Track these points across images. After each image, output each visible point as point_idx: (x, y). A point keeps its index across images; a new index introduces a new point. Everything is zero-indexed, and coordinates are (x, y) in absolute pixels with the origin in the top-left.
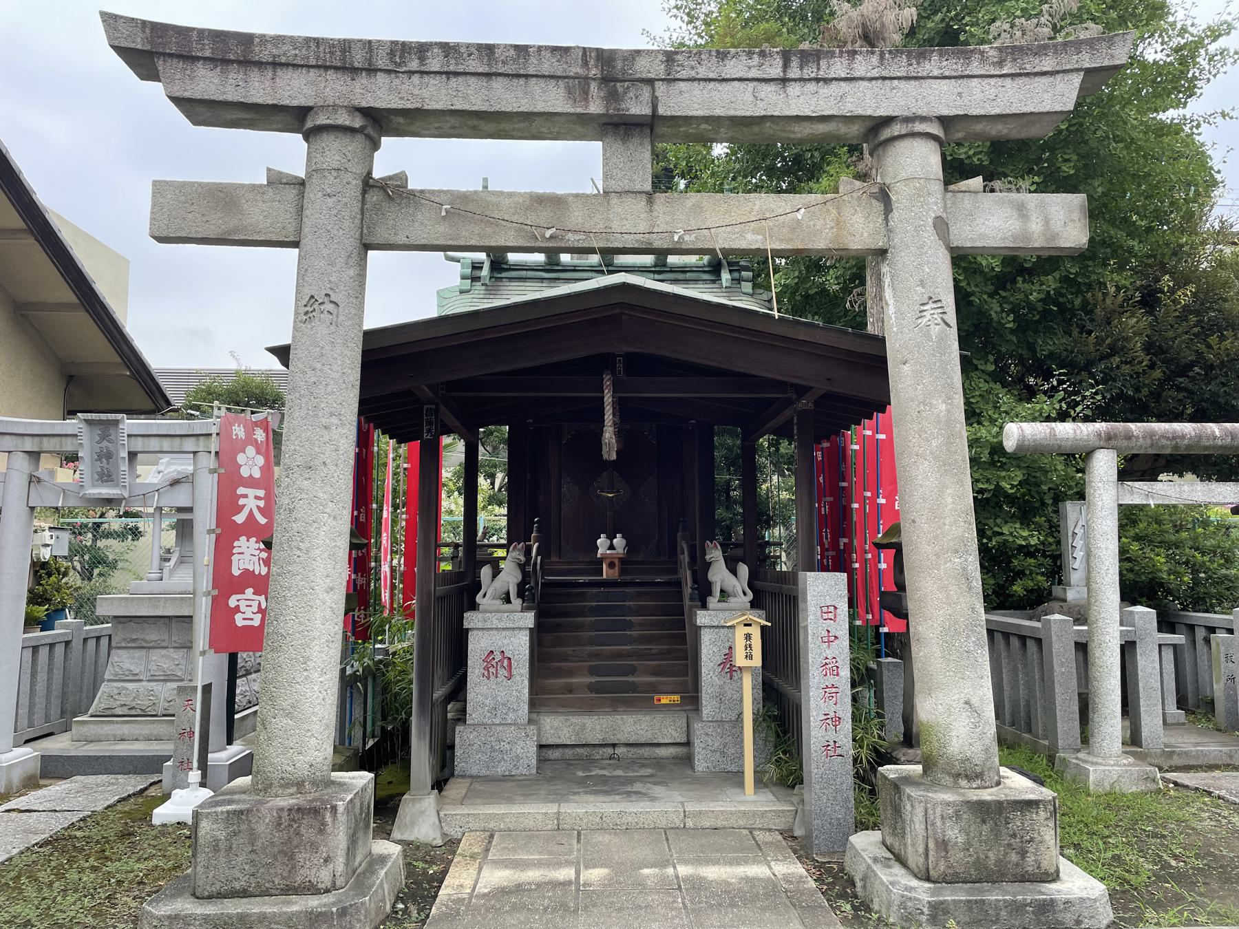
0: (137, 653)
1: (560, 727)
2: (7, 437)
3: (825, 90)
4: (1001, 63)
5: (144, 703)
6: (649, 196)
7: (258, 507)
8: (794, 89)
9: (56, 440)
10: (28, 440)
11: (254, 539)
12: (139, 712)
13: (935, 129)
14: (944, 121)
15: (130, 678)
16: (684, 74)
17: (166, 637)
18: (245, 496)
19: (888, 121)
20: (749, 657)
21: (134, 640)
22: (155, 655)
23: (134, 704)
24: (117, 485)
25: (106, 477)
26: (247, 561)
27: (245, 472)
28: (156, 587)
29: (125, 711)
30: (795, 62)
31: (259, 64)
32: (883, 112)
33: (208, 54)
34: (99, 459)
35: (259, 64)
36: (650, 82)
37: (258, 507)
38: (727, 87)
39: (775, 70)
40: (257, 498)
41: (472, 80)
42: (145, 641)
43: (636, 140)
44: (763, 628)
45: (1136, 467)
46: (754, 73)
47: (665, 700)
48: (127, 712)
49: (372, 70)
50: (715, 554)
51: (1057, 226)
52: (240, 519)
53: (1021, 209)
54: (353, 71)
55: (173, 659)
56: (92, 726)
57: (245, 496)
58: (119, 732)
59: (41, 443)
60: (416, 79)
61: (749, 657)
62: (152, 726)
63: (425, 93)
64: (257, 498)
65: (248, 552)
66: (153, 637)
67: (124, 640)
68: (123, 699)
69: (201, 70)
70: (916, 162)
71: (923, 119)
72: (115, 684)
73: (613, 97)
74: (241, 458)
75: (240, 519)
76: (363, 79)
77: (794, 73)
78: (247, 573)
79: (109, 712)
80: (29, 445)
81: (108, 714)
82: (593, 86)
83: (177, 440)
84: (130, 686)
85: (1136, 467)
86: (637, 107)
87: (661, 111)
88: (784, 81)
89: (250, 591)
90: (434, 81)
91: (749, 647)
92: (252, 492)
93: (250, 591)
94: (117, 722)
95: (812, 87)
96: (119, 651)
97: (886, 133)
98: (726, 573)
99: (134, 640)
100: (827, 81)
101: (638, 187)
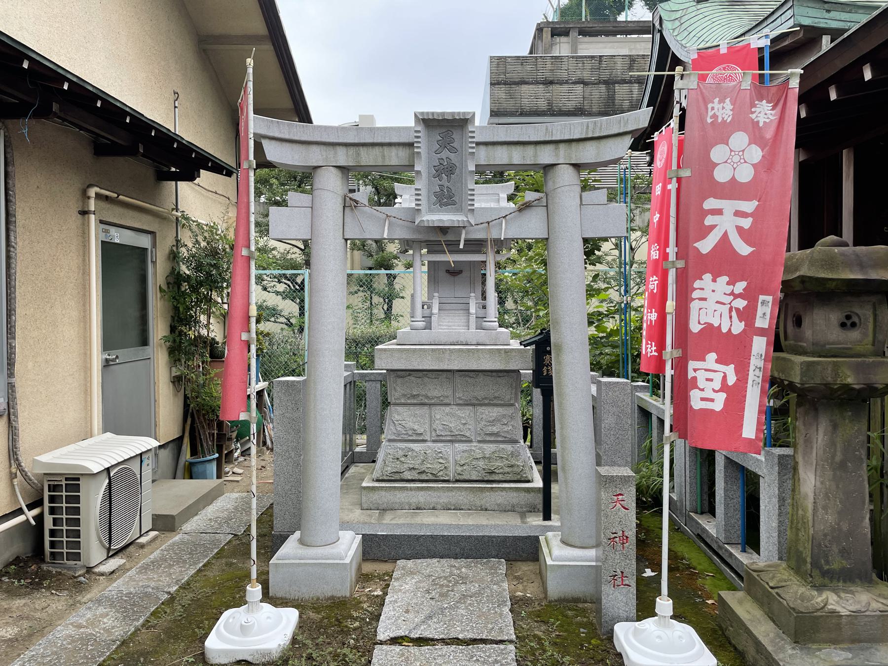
0: (418, 410)
2: (315, 148)
5: (433, 466)
7: (740, 229)
9: (377, 150)
10: (341, 151)
11: (725, 279)
12: (431, 477)
15: (414, 438)
17: (449, 393)
18: (719, 212)
21: (414, 396)
22: (439, 413)
23: (423, 468)
24: (460, 210)
25: (445, 198)
26: (710, 312)
27: (722, 175)
28: (425, 335)
34: (438, 175)
37: (740, 229)
40: (738, 214)
42: (427, 397)
48: (417, 477)
52: (705, 246)
55: (460, 418)
56: (383, 493)
57: (719, 212)
58: (414, 500)
59: (358, 154)
62: (450, 494)
64: (738, 214)
65: (713, 298)
66: (436, 393)
67: (404, 395)
68: (410, 462)
72: (400, 445)
74: (717, 154)
75: (705, 246)
78: (710, 330)
79: (397, 477)
80: (343, 157)
81: (395, 478)
83: (530, 150)
89: (712, 357)
92: (728, 206)
93: (712, 357)
94: (411, 489)
96: (399, 408)
99: (414, 396)
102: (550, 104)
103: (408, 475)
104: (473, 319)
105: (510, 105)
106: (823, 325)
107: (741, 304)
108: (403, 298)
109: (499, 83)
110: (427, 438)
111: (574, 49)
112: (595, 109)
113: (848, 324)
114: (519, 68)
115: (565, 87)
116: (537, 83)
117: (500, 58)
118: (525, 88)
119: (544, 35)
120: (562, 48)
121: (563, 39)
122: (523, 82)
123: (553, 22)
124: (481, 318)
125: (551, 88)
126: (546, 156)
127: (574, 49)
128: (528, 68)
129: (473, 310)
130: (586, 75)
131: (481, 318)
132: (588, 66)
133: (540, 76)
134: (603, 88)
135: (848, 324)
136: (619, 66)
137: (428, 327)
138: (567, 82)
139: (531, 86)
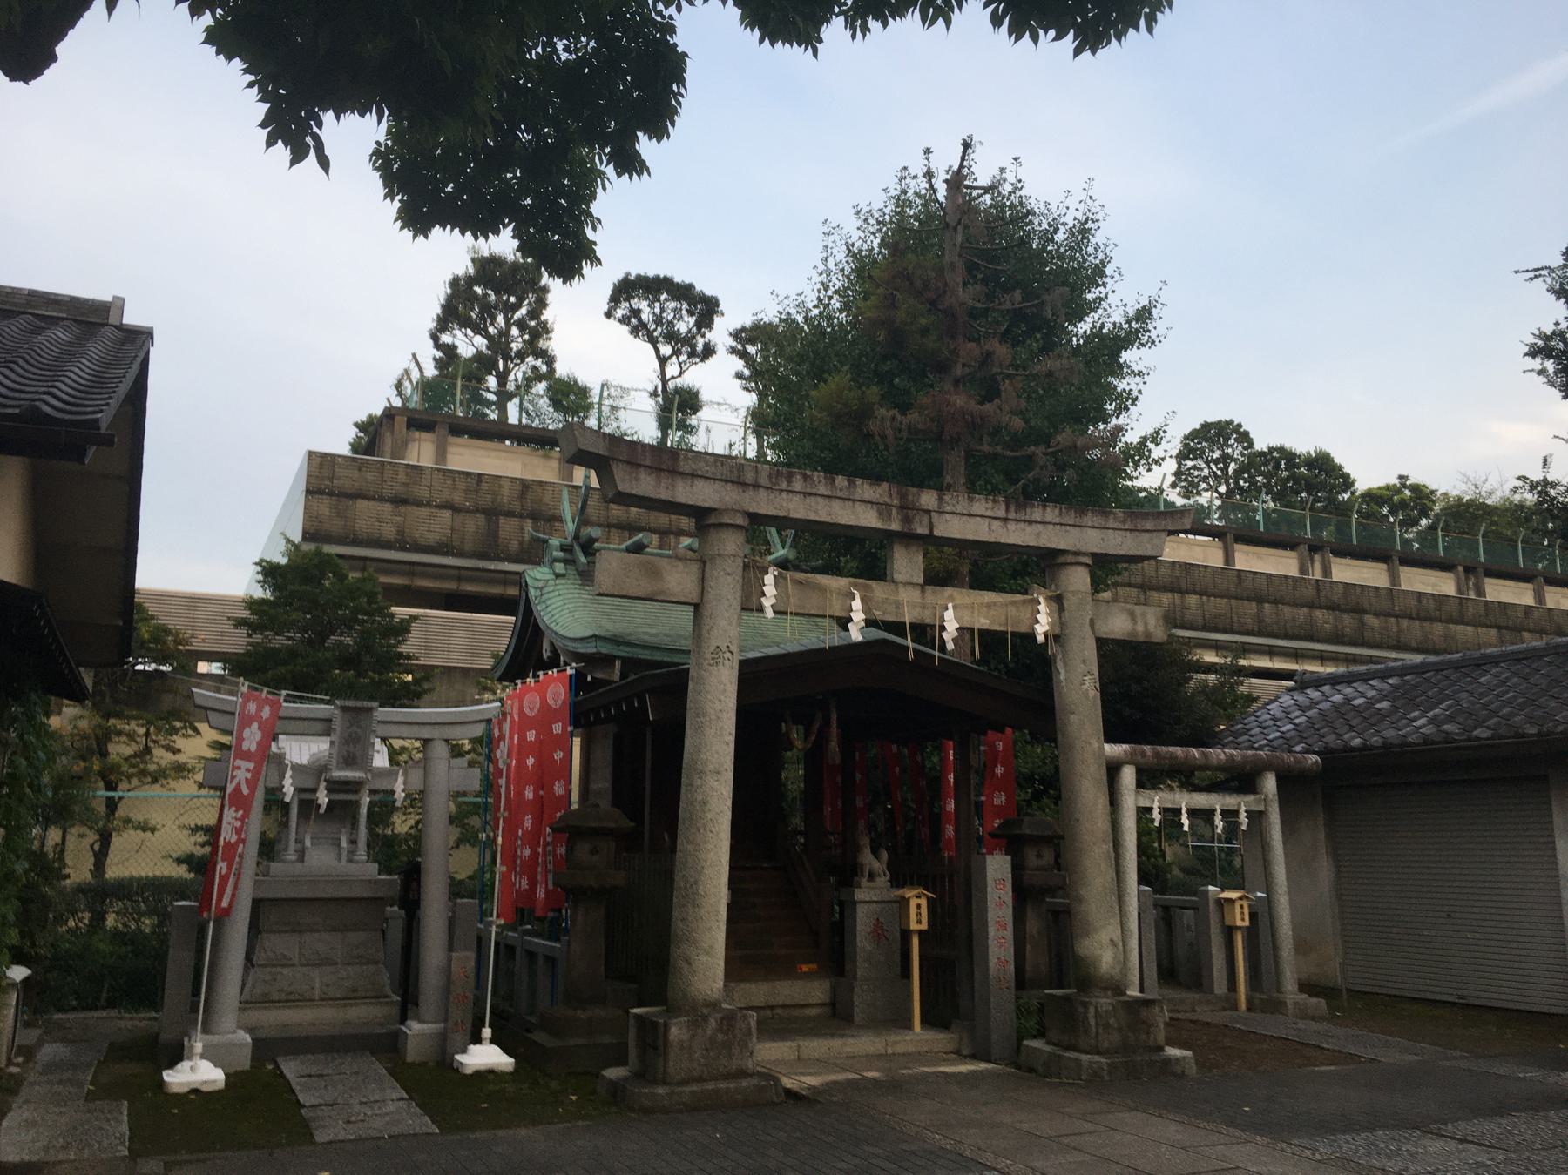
1: (758, 992)
3: (1029, 529)
4: (1124, 522)
6: (922, 587)
8: (1012, 526)
13: (1088, 560)
14: (1094, 555)
16: (948, 509)
19: (1063, 552)
20: (919, 922)
29: (283, 997)
30: (1013, 508)
31: (681, 474)
32: (1061, 547)
33: (648, 463)
35: (681, 474)
36: (928, 512)
38: (972, 520)
39: (1001, 513)
41: (820, 499)
43: (914, 548)
44: (929, 899)
45: (1148, 779)
46: (988, 513)
47: (805, 968)
49: (756, 486)
50: (865, 841)
51: (1151, 628)
53: (1132, 615)
54: (742, 484)
60: (784, 495)
61: (919, 922)
63: (791, 506)
69: (643, 475)
70: (1077, 580)
71: (1085, 554)
73: (907, 520)
76: (750, 492)
77: (1012, 515)
82: (894, 511)
84: (286, 971)
85: (1148, 779)
86: (922, 530)
87: (936, 533)
88: (1006, 520)
90: (797, 498)
91: (919, 914)
95: (1022, 525)
97: (1061, 559)
98: (871, 857)
100: (1030, 522)
101: (915, 580)
102: (401, 532)
103: (275, 997)
104: (344, 853)
105: (336, 527)
106: (583, 850)
107: (238, 824)
108: (145, 827)
109: (320, 492)
110: (296, 961)
111: (441, 455)
112: (468, 547)
113: (594, 851)
114: (356, 474)
115: (424, 512)
116: (382, 499)
117: (324, 456)
118: (362, 504)
119: (397, 427)
120: (421, 452)
121: (424, 435)
122: (359, 495)
123: (415, 410)
124: (352, 853)
125: (403, 509)
126: (426, 733)
127: (441, 455)
128: (370, 476)
129: (344, 844)
130: (457, 498)
131: (352, 853)
132: (461, 486)
133: (387, 489)
134: (481, 519)
135: (594, 851)
136: (506, 491)
137: (301, 859)
138: (429, 504)
139: (372, 503)
